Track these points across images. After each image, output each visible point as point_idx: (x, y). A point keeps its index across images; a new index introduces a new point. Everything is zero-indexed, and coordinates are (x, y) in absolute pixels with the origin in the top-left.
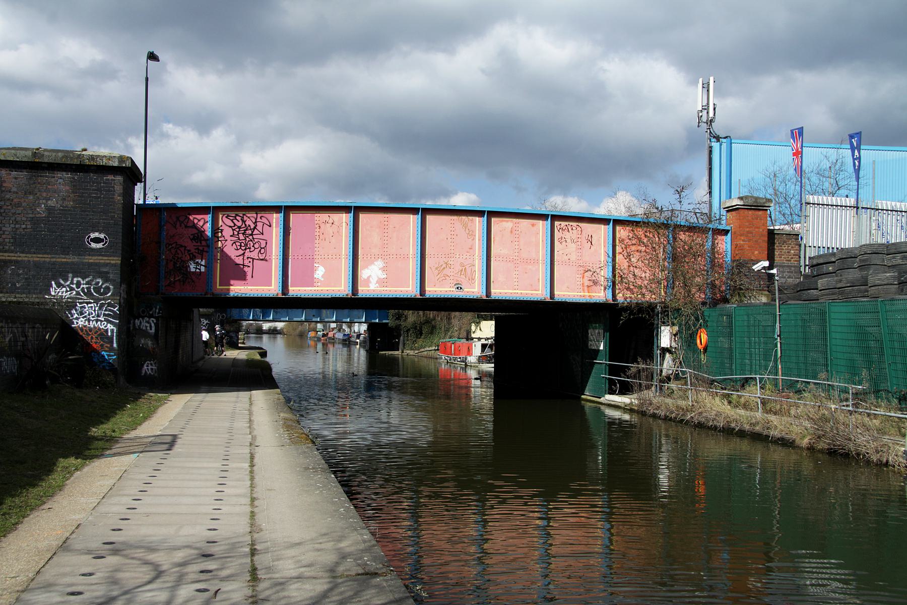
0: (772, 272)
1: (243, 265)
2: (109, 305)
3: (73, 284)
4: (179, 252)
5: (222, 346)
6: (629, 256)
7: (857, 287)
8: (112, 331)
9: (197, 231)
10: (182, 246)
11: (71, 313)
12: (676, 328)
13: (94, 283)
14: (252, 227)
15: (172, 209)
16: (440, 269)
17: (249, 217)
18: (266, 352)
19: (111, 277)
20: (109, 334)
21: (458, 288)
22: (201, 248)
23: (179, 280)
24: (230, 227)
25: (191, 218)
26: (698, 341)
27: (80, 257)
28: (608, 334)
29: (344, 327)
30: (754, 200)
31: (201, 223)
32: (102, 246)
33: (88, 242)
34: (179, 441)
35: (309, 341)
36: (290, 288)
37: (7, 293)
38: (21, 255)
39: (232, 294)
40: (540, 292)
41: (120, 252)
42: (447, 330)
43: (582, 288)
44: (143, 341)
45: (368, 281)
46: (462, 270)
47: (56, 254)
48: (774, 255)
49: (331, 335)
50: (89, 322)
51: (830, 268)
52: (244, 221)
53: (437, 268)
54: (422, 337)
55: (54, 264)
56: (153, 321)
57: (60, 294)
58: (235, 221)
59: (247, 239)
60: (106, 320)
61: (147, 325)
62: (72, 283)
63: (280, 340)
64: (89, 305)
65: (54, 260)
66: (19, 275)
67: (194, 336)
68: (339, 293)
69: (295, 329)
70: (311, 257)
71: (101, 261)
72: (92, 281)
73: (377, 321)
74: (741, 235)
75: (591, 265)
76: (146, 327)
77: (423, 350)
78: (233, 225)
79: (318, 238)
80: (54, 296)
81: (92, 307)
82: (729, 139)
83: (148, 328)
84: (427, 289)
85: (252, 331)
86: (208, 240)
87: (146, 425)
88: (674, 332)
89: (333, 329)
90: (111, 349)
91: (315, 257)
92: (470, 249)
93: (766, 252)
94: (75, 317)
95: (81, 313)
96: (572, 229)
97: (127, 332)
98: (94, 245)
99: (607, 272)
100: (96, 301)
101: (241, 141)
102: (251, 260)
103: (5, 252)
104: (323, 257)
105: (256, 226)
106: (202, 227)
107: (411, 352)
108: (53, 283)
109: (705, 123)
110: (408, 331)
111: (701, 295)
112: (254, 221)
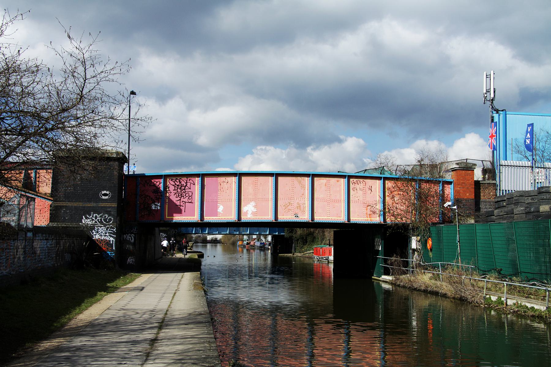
0: (454, 207)
1: (180, 205)
2: (111, 227)
3: (93, 217)
4: (146, 199)
5: (174, 250)
6: (393, 197)
7: (509, 215)
8: (113, 241)
9: (156, 188)
10: (148, 196)
11: (92, 232)
12: (419, 238)
13: (104, 216)
14: (185, 185)
15: (142, 177)
16: (286, 206)
17: (183, 180)
18: (203, 254)
19: (112, 214)
20: (111, 243)
21: (296, 216)
22: (158, 197)
23: (147, 214)
24: (173, 185)
25: (153, 181)
26: (428, 245)
27: (97, 203)
28: (383, 241)
29: (262, 238)
30: (465, 165)
31: (158, 184)
32: (108, 198)
33: (101, 196)
34: (145, 289)
35: (238, 247)
36: (205, 218)
37: (61, 222)
38: (68, 203)
39: (174, 221)
40: (342, 218)
41: (117, 200)
42: (323, 239)
43: (366, 215)
44: (127, 246)
45: (246, 213)
46: (298, 206)
47: (85, 202)
48: (480, 195)
49: (252, 243)
50: (101, 237)
51: (504, 204)
52: (180, 182)
53: (284, 206)
54: (307, 244)
55: (84, 207)
56: (133, 236)
57: (87, 222)
58: (176, 182)
59: (182, 192)
60: (109, 235)
61: (130, 237)
62: (93, 217)
63: (219, 247)
64: (101, 228)
65: (84, 205)
66: (67, 213)
67: (156, 244)
68: (231, 220)
69: (229, 240)
70: (216, 201)
71: (108, 205)
72: (103, 215)
73: (277, 233)
74: (458, 185)
75: (371, 203)
76: (129, 239)
77: (306, 253)
78: (174, 184)
79: (219, 190)
80: (84, 223)
81: (102, 229)
82: (504, 112)
83: (130, 239)
84: (279, 217)
85: (199, 241)
86: (161, 192)
87: (131, 284)
88: (418, 240)
89: (254, 239)
90: (112, 250)
91: (218, 200)
92: (303, 195)
93: (474, 194)
94: (94, 234)
95: (97, 232)
96: (360, 183)
97: (119, 241)
98: (104, 197)
99: (380, 207)
100: (105, 226)
101: (190, 107)
102: (184, 203)
103: (61, 202)
104: (222, 200)
105: (187, 184)
106: (158, 186)
107: (299, 255)
108: (84, 217)
109: (488, 101)
110: (298, 240)
111: (436, 219)
112: (186, 182)
